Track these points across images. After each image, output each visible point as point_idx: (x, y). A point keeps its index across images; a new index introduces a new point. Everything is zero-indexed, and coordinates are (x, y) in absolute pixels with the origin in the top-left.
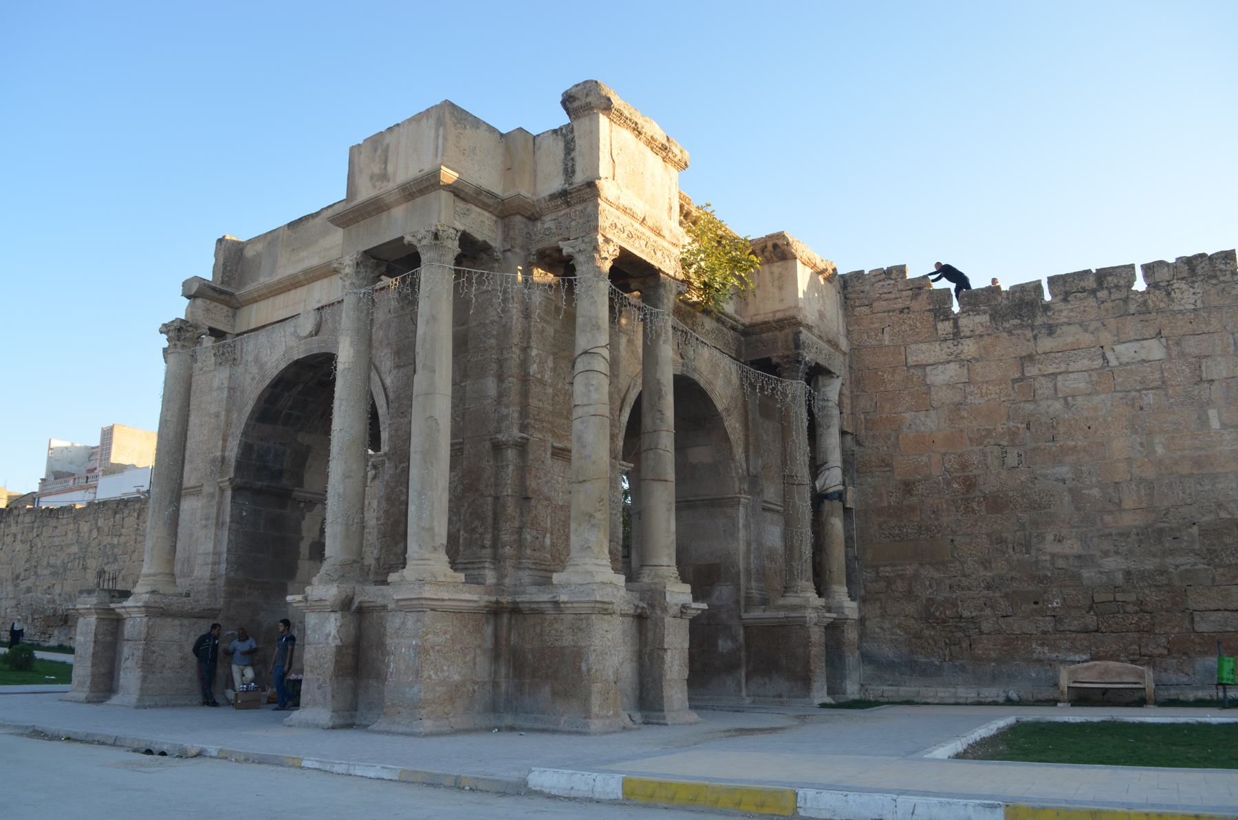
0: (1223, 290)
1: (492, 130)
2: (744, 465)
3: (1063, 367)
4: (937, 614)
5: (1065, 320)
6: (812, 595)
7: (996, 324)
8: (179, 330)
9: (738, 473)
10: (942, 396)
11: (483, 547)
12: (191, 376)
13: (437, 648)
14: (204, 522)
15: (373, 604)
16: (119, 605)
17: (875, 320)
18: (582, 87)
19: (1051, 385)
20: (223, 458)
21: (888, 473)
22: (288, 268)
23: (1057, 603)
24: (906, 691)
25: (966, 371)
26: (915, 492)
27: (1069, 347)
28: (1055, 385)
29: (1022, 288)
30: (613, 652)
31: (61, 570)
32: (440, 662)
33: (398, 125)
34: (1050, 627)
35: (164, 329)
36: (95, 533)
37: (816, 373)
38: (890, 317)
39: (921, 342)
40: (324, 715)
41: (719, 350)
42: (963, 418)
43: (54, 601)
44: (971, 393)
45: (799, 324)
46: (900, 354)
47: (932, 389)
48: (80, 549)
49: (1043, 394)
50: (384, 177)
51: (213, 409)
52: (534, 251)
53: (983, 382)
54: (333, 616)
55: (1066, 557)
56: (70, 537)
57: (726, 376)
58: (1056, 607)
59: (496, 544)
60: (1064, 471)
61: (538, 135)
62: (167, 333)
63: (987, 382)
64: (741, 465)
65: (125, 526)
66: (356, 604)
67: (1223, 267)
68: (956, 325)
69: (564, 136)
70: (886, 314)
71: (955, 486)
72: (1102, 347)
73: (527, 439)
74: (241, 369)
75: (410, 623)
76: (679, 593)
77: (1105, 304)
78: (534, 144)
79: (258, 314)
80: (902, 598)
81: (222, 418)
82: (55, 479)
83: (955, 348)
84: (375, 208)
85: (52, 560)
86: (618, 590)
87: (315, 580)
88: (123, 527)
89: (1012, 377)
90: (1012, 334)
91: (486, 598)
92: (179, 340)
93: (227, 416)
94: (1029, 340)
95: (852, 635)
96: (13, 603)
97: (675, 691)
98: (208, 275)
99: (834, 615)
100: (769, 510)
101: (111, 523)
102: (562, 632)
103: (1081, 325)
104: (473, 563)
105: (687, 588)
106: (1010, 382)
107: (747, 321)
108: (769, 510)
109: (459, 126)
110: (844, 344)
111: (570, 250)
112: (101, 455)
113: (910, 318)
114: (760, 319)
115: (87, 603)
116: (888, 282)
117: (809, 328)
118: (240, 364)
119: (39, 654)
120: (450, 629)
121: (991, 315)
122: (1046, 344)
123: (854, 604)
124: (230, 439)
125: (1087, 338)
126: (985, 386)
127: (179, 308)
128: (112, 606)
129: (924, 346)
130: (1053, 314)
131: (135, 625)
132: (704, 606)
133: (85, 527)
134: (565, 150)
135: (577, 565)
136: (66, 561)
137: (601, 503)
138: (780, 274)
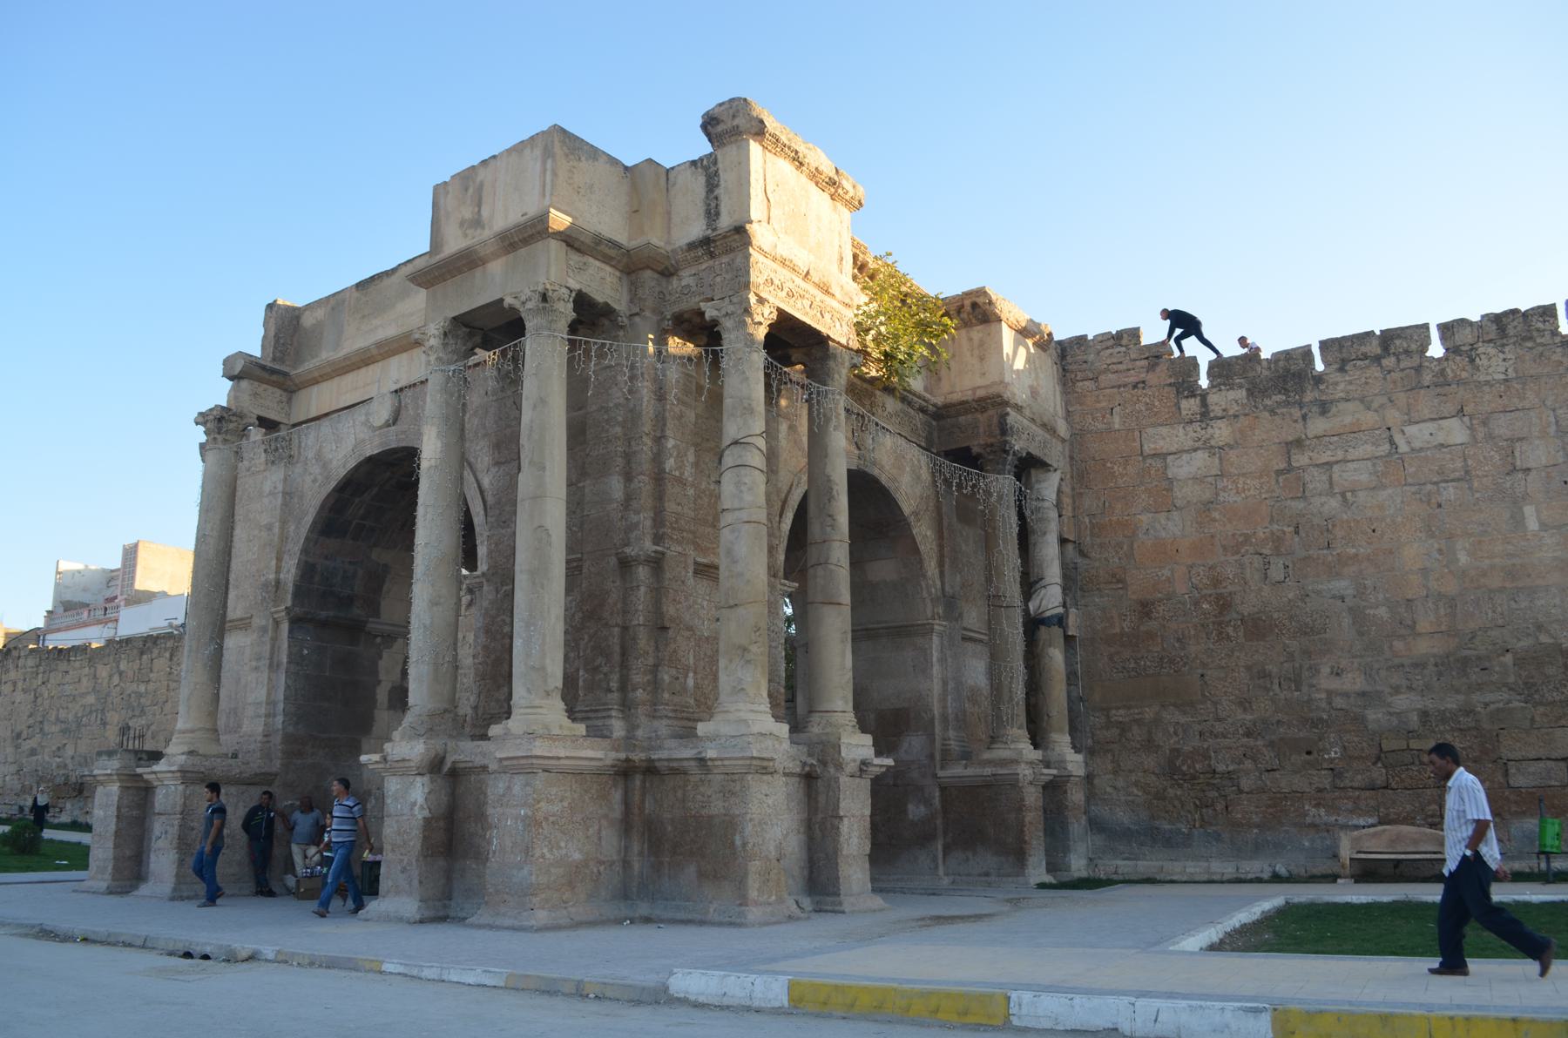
0: (1541, 355)
1: (614, 162)
2: (938, 583)
3: (1340, 455)
4: (1185, 768)
5: (1342, 395)
8: (220, 420)
9: (930, 593)
10: (1186, 493)
12: (235, 479)
13: (551, 819)
14: (254, 664)
15: (470, 765)
17: (1101, 398)
19: (1324, 478)
20: (278, 582)
21: (1121, 592)
22: (357, 339)
23: (1336, 753)
26: (1154, 615)
28: (1331, 477)
30: (775, 821)
31: (74, 726)
32: (555, 837)
33: (494, 157)
35: (201, 420)
36: (116, 679)
37: (1028, 466)
38: (1120, 393)
40: (409, 906)
42: (1214, 520)
43: (65, 766)
44: (1224, 489)
45: (1006, 403)
46: (1134, 440)
48: (98, 699)
49: (1315, 488)
50: (477, 223)
51: (265, 519)
55: (1346, 695)
58: (1334, 759)
59: (624, 687)
60: (1342, 585)
61: (673, 168)
62: (204, 424)
63: (1244, 475)
67: (1540, 325)
68: (1204, 403)
69: (706, 169)
70: (1115, 390)
72: (1389, 429)
74: (298, 469)
76: (857, 746)
77: (1392, 373)
81: (276, 530)
83: (1203, 432)
84: (467, 262)
85: (63, 714)
86: (781, 743)
87: (396, 735)
88: (151, 671)
89: (1276, 468)
92: (219, 433)
93: (282, 528)
94: (1296, 421)
95: (1076, 796)
96: (13, 768)
97: (854, 871)
99: (1054, 772)
101: (136, 666)
103: (1362, 401)
105: (868, 739)
106: (1274, 475)
107: (939, 401)
109: (572, 157)
110: (1062, 428)
112: (123, 580)
113: (1146, 395)
114: (956, 397)
115: (107, 767)
117: (1018, 408)
118: (297, 462)
121: (1248, 390)
122: (1318, 425)
123: (1079, 758)
125: (1369, 418)
127: (219, 393)
128: (139, 770)
129: (1164, 430)
130: (1327, 387)
132: (890, 762)
133: (103, 672)
134: (707, 186)
136: (80, 715)
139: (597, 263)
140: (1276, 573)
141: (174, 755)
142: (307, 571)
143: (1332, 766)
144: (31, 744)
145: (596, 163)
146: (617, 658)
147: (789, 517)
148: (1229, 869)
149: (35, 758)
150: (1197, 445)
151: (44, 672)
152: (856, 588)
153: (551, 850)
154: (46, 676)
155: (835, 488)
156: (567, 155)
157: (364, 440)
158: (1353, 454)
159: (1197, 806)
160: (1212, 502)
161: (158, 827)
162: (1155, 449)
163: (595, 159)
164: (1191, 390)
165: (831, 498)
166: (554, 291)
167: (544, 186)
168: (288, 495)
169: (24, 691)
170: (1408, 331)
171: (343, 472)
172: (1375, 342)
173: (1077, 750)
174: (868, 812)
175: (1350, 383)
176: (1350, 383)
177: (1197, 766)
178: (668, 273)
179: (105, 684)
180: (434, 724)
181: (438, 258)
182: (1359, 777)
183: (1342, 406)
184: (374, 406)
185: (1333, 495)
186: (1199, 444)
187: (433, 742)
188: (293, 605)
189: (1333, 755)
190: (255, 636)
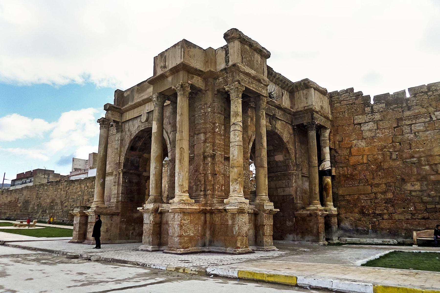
1: (200, 48)
2: (295, 161)
3: (414, 122)
4: (366, 212)
6: (320, 207)
7: (388, 107)
8: (103, 121)
9: (292, 164)
10: (367, 134)
11: (201, 191)
12: (108, 136)
13: (185, 225)
14: (114, 184)
15: (165, 210)
16: (86, 211)
17: (342, 108)
18: (230, 31)
19: (409, 128)
20: (119, 162)
21: (348, 163)
22: (138, 99)
23: (412, 208)
24: (354, 240)
25: (376, 125)
26: (357, 169)
27: (416, 114)
28: (411, 128)
29: (398, 93)
30: (245, 226)
32: (186, 230)
33: (169, 49)
34: (410, 217)
35: (98, 121)
36: (86, 188)
37: (320, 129)
38: (347, 107)
39: (359, 115)
41: (285, 121)
42: (375, 142)
45: (314, 111)
46: (351, 120)
47: (363, 132)
48: (82, 193)
49: (406, 132)
50: (165, 67)
51: (116, 147)
52: (216, 89)
53: (383, 129)
55: (415, 191)
56: (78, 189)
57: (287, 130)
58: (412, 210)
59: (205, 190)
61: (217, 49)
62: (99, 122)
63: (384, 128)
64: (293, 161)
68: (372, 108)
69: (225, 49)
70: (346, 106)
72: (430, 113)
73: (215, 154)
74: (124, 133)
75: (176, 216)
76: (269, 206)
77: (431, 97)
78: (215, 52)
79: (128, 116)
80: (353, 207)
81: (119, 150)
82: (75, 170)
83: (372, 116)
84: (163, 77)
85: (73, 197)
86: (247, 205)
87: (147, 202)
89: (394, 126)
90: (394, 110)
92: (103, 125)
93: (120, 149)
94: (400, 112)
95: (335, 220)
97: (268, 240)
99: (327, 213)
100: (304, 176)
101: (91, 185)
102: (227, 219)
103: (421, 106)
104: (198, 196)
105: (272, 204)
106: (393, 128)
107: (294, 110)
108: (304, 176)
109: (189, 47)
110: (330, 116)
111: (228, 89)
112: (89, 163)
113: (355, 107)
114: (299, 109)
115: (76, 211)
116: (346, 94)
117: (317, 112)
118: (124, 132)
120: (190, 218)
121: (386, 104)
123: (336, 209)
124: (121, 156)
125: (424, 110)
126: (383, 130)
127: (103, 114)
129: (360, 117)
130: (410, 102)
133: (83, 186)
134: (226, 54)
135: (232, 196)
137: (240, 175)
138: (306, 93)
139: (197, 76)
140: (394, 157)
141: (93, 207)
143: (411, 212)
145: (195, 49)
146: (203, 182)
147: (251, 144)
148: (380, 241)
150: (370, 120)
151: (68, 186)
152: (269, 163)
153: (185, 233)
154: (69, 187)
155: (263, 135)
156: (187, 47)
157: (140, 126)
158: (418, 121)
159: (370, 223)
160: (374, 137)
162: (358, 122)
163: (195, 48)
164: (369, 105)
165: (261, 138)
166: (184, 84)
167: (181, 56)
169: (64, 191)
170: (436, 84)
172: (425, 88)
173: (335, 206)
175: (417, 100)
176: (417, 100)
177: (370, 212)
178: (216, 79)
179: (83, 189)
181: (155, 77)
182: (420, 216)
183: (415, 107)
185: (412, 133)
187: (156, 204)
188: (123, 169)
189: (412, 209)
190: (114, 177)
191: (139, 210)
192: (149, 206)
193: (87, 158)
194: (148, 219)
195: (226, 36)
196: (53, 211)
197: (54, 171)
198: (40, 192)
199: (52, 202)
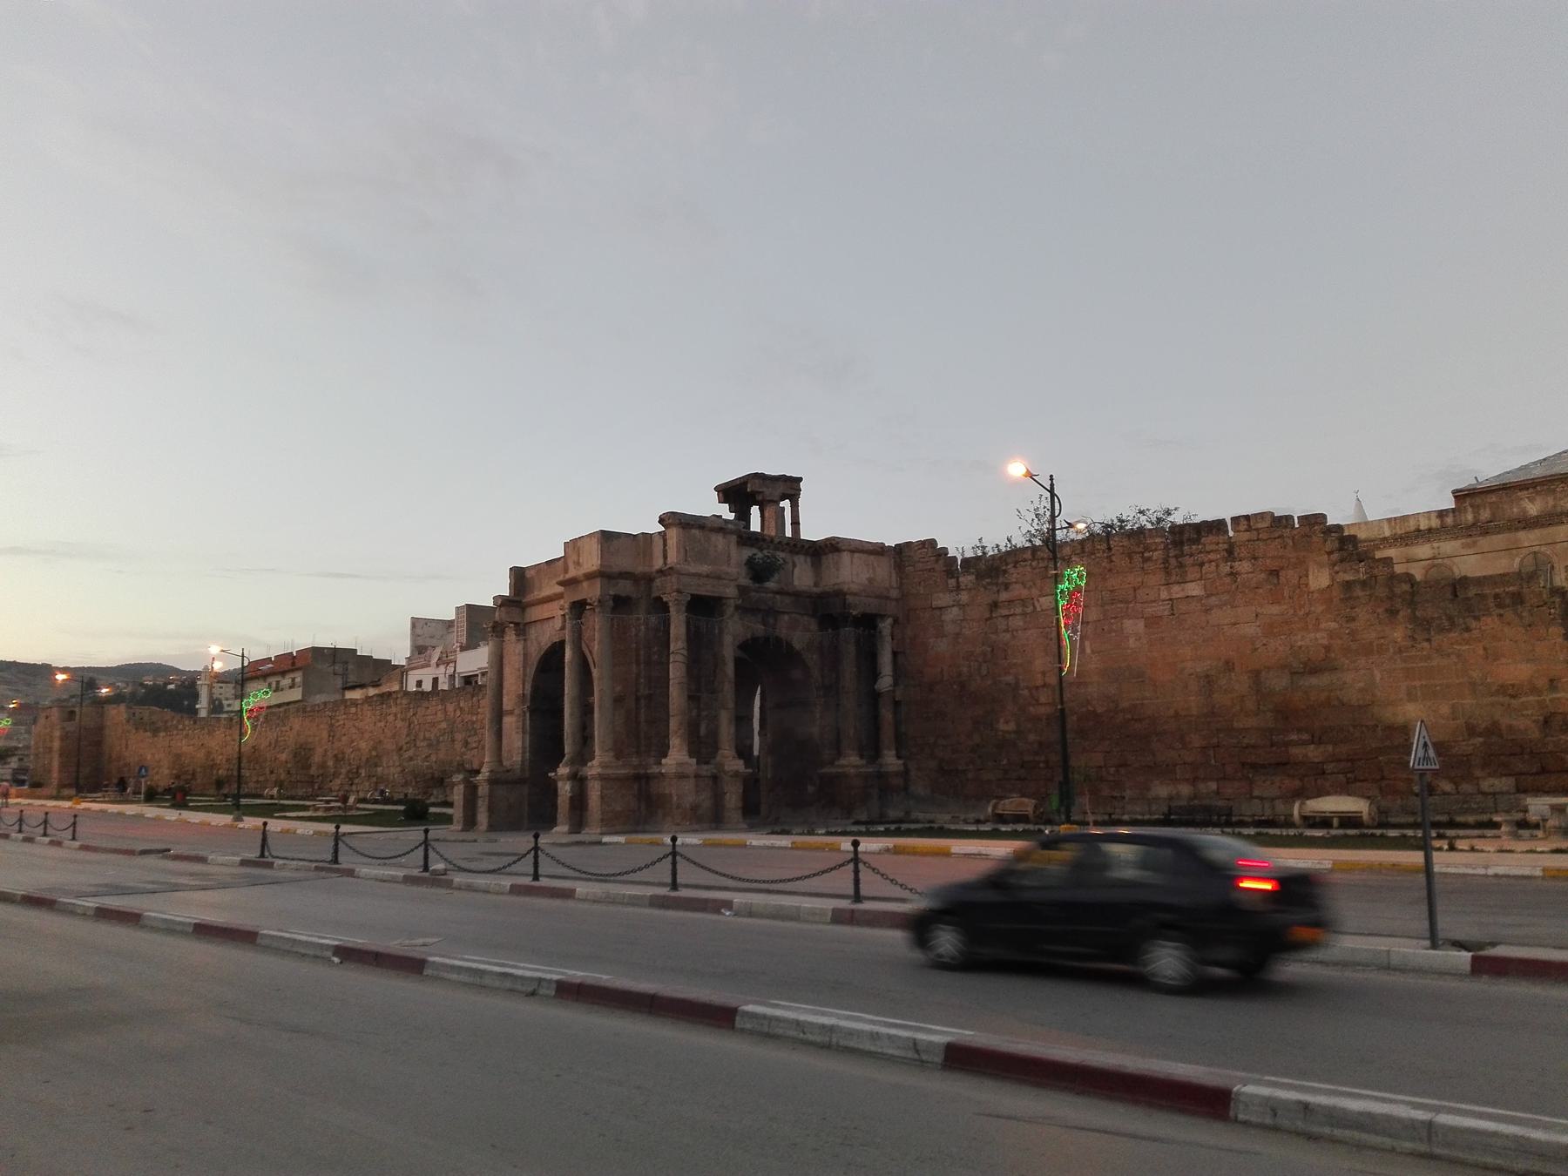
0: (1098, 563)
5: (1014, 580)
10: (950, 628)
20: (523, 694)
31: (435, 743)
36: (458, 713)
40: (565, 828)
43: (432, 768)
44: (965, 627)
45: (845, 594)
54: (568, 782)
60: (1010, 679)
65: (481, 706)
66: (579, 776)
67: (1099, 547)
71: (955, 687)
81: (521, 672)
85: (427, 735)
87: (561, 765)
88: (479, 707)
91: (632, 772)
96: (399, 769)
98: (506, 593)
103: (1022, 583)
119: (432, 810)
122: (1004, 596)
128: (471, 779)
129: (941, 595)
131: (483, 790)
132: (750, 770)
133: (450, 708)
136: (438, 735)
142: (535, 689)
144: (410, 753)
149: (412, 763)
161: (480, 802)
163: (620, 538)
168: (525, 655)
169: (403, 720)
171: (546, 648)
174: (741, 791)
180: (572, 762)
184: (555, 620)
186: (955, 603)
191: (550, 777)
192: (563, 770)
193: (451, 616)
194: (565, 789)
195: (661, 521)
196: (380, 769)
197: (356, 650)
198: (338, 721)
199: (375, 748)
